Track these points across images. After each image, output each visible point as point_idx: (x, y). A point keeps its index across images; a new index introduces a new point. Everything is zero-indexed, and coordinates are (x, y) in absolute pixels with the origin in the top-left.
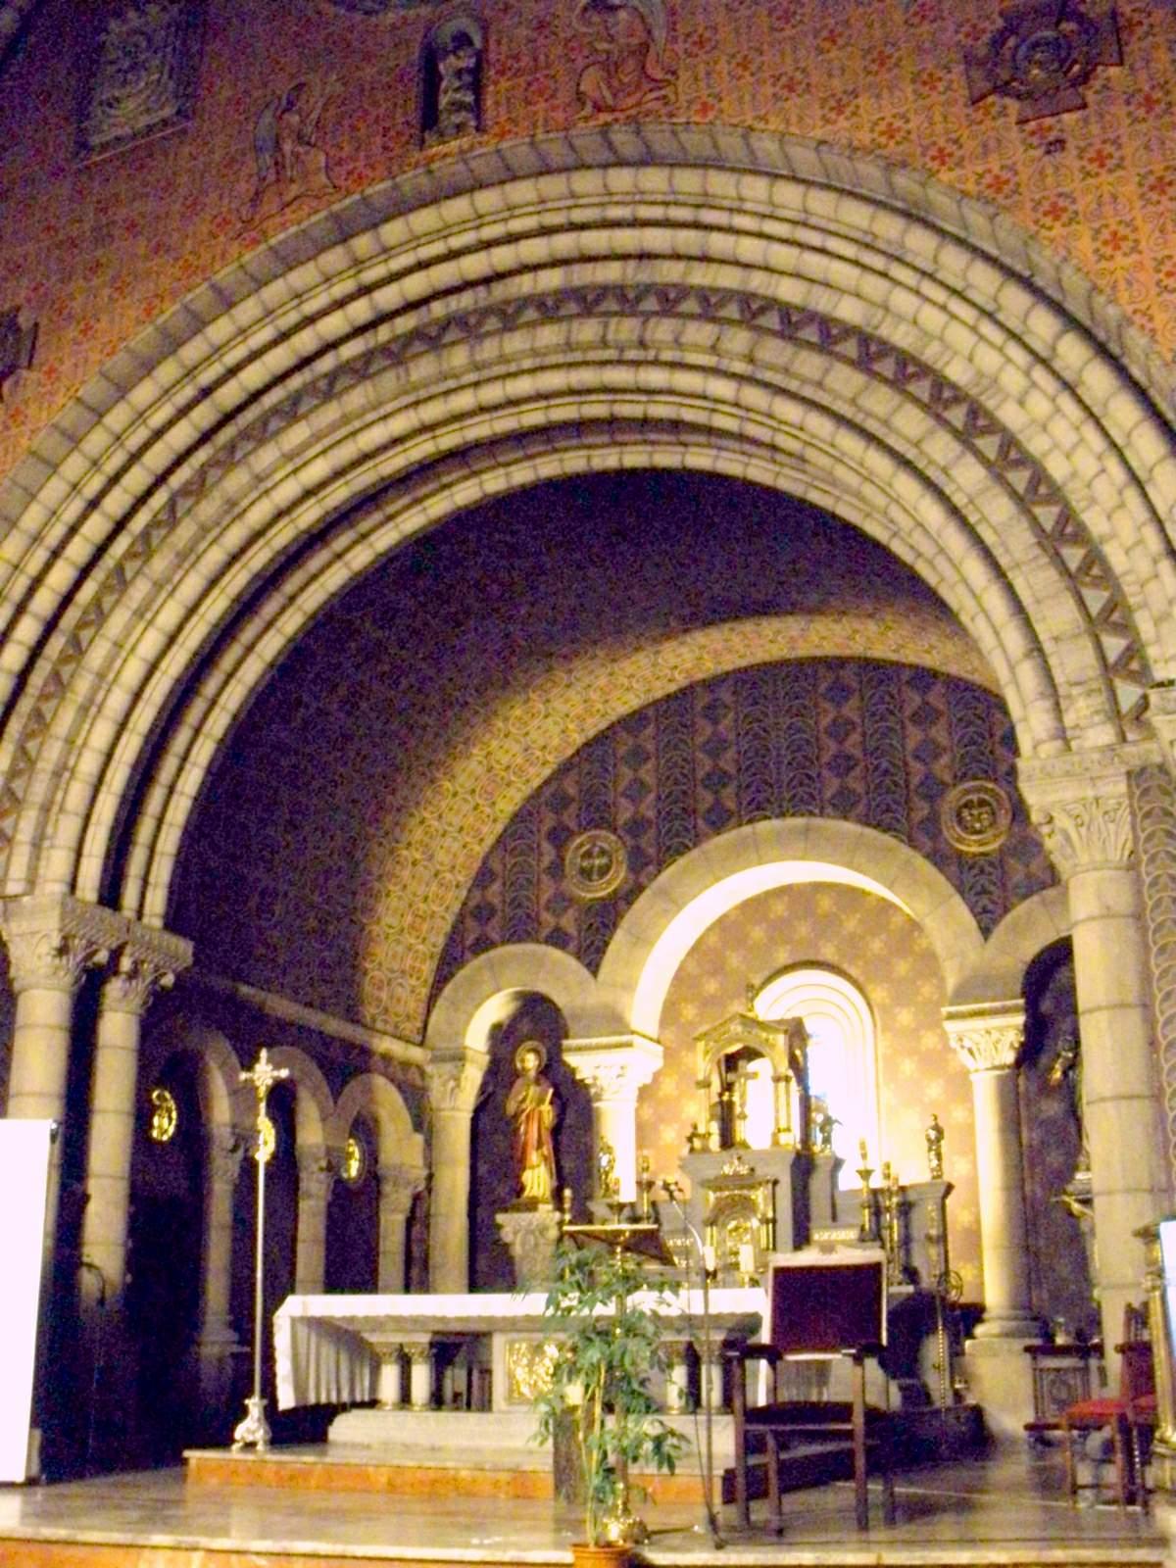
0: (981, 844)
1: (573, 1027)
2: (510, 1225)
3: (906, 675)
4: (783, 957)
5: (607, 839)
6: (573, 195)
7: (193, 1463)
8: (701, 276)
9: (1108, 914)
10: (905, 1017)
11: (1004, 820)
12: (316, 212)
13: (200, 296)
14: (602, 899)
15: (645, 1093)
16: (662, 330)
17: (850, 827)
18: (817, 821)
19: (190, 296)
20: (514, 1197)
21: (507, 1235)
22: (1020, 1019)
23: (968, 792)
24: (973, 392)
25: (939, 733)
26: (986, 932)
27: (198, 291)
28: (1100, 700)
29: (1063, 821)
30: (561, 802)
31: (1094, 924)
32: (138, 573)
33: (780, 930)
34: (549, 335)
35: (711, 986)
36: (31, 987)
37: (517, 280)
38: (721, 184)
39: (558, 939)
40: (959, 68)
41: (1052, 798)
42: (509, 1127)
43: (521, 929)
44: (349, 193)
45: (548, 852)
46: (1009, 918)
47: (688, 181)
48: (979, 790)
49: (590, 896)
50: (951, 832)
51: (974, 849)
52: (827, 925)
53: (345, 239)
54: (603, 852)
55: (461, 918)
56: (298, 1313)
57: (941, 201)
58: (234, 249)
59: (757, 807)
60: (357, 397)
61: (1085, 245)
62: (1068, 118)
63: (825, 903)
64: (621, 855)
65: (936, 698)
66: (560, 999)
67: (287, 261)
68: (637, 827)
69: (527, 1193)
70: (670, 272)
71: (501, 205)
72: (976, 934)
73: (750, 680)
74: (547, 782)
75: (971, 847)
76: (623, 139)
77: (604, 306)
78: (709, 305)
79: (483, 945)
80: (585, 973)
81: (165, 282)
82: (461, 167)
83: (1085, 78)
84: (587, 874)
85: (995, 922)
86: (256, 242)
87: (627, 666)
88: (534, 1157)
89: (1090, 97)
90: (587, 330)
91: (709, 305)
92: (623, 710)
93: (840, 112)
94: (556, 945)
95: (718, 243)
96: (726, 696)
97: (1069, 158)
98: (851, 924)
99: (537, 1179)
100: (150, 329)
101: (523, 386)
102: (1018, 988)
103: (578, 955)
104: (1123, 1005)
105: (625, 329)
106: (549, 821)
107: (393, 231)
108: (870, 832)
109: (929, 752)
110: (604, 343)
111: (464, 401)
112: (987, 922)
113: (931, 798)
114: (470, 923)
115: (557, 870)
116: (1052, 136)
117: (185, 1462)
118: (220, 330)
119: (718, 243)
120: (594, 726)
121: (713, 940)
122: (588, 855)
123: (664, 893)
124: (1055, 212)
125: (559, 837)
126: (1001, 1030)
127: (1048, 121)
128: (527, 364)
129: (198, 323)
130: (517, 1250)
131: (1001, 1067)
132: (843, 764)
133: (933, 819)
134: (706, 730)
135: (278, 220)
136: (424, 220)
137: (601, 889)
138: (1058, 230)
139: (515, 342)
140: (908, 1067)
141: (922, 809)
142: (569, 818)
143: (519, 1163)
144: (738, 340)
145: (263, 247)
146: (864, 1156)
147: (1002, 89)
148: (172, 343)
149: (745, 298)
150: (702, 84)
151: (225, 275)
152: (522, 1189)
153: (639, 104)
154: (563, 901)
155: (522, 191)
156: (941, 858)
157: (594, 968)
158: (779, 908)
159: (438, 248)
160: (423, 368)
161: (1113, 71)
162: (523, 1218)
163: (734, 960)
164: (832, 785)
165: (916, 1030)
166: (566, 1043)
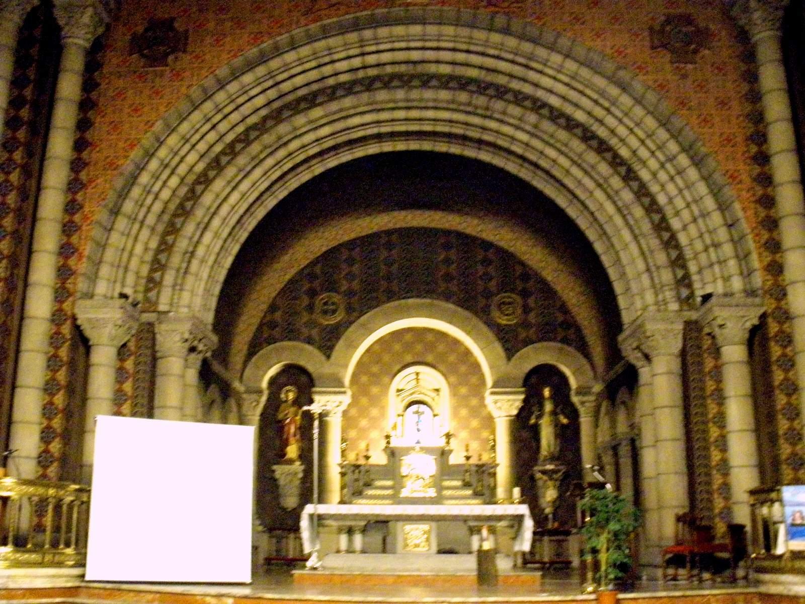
0: (509, 320)
1: (317, 382)
2: (280, 470)
3: (480, 242)
4: (409, 358)
5: (336, 298)
6: (471, 38)
7: (296, 576)
8: (515, 85)
9: (669, 373)
10: (463, 390)
11: (519, 311)
12: (347, 13)
13: (283, 38)
14: (332, 325)
15: (345, 413)
16: (499, 105)
17: (451, 306)
18: (436, 302)
19: (278, 38)
20: (281, 457)
21: (277, 475)
22: (522, 397)
23: (504, 297)
24: (629, 162)
25: (491, 270)
26: (509, 358)
27: (284, 36)
28: (673, 293)
29: (658, 337)
30: (312, 277)
31: (665, 376)
32: (229, 163)
33: (408, 347)
34: (444, 95)
35: (375, 369)
36: (169, 356)
37: (429, 65)
38: (541, 52)
39: (309, 341)
40: (646, 34)
41: (655, 327)
42: (280, 427)
43: (291, 334)
44: (365, 9)
45: (306, 301)
46: (518, 354)
47: (527, 47)
48: (509, 297)
49: (327, 323)
50: (496, 314)
51: (504, 322)
52: (430, 347)
53: (684, 150)
54: (333, 304)
55: (261, 326)
56: (312, 512)
57: (638, 87)
58: (303, 21)
59: (407, 293)
60: (348, 102)
61: (694, 121)
62: (690, 66)
63: (430, 337)
64: (342, 307)
65: (491, 254)
66: (310, 368)
67: (326, 33)
68: (350, 293)
69: (287, 457)
70: (502, 80)
71: (436, 33)
72: (504, 360)
73: (407, 234)
74: (305, 267)
75: (503, 321)
76: (500, 21)
77: (489, 92)
78: (519, 99)
79: (271, 340)
80: (323, 358)
81: (264, 27)
82: (420, 12)
83: (695, 52)
84: (325, 312)
85: (513, 356)
86: (315, 21)
87: (360, 222)
88: (292, 440)
89: (698, 59)
90: (463, 97)
91: (519, 99)
92: (346, 238)
93: (599, 37)
94: (309, 343)
95: (532, 75)
96: (394, 237)
97: (689, 82)
98: (441, 347)
99: (292, 451)
100: (255, 50)
101: (430, 114)
102: (521, 382)
103: (320, 348)
104: (675, 407)
105: (481, 100)
106: (307, 286)
107: (383, 32)
108: (459, 309)
109: (487, 277)
110: (469, 104)
111: (401, 114)
112: (510, 353)
113: (487, 298)
114: (265, 328)
115: (310, 308)
116: (683, 72)
117: (292, 575)
118: (290, 57)
119: (532, 75)
120: (334, 244)
121: (377, 347)
122: (326, 304)
123: (363, 325)
124: (683, 104)
125: (312, 293)
126: (515, 400)
127: (682, 65)
128: (431, 104)
129: (278, 51)
130: (282, 482)
131: (510, 416)
132: (448, 277)
133: (488, 306)
134: (384, 254)
135: (327, 12)
136: (399, 30)
137: (332, 321)
138: (684, 112)
139: (429, 94)
140: (464, 412)
141: (482, 302)
142: (316, 284)
143: (286, 443)
144: (532, 118)
145: (318, 24)
146: (467, 451)
147: (664, 46)
148: (263, 59)
149: (535, 100)
150: (538, 7)
151: (298, 32)
152: (285, 455)
153: (508, 7)
154: (311, 324)
155: (449, 30)
156: (491, 324)
157: (328, 357)
158: (408, 337)
159: (403, 45)
160: (382, 95)
161: (707, 52)
162: (286, 468)
163: (386, 358)
164: (443, 286)
165: (469, 396)
166: (314, 389)
